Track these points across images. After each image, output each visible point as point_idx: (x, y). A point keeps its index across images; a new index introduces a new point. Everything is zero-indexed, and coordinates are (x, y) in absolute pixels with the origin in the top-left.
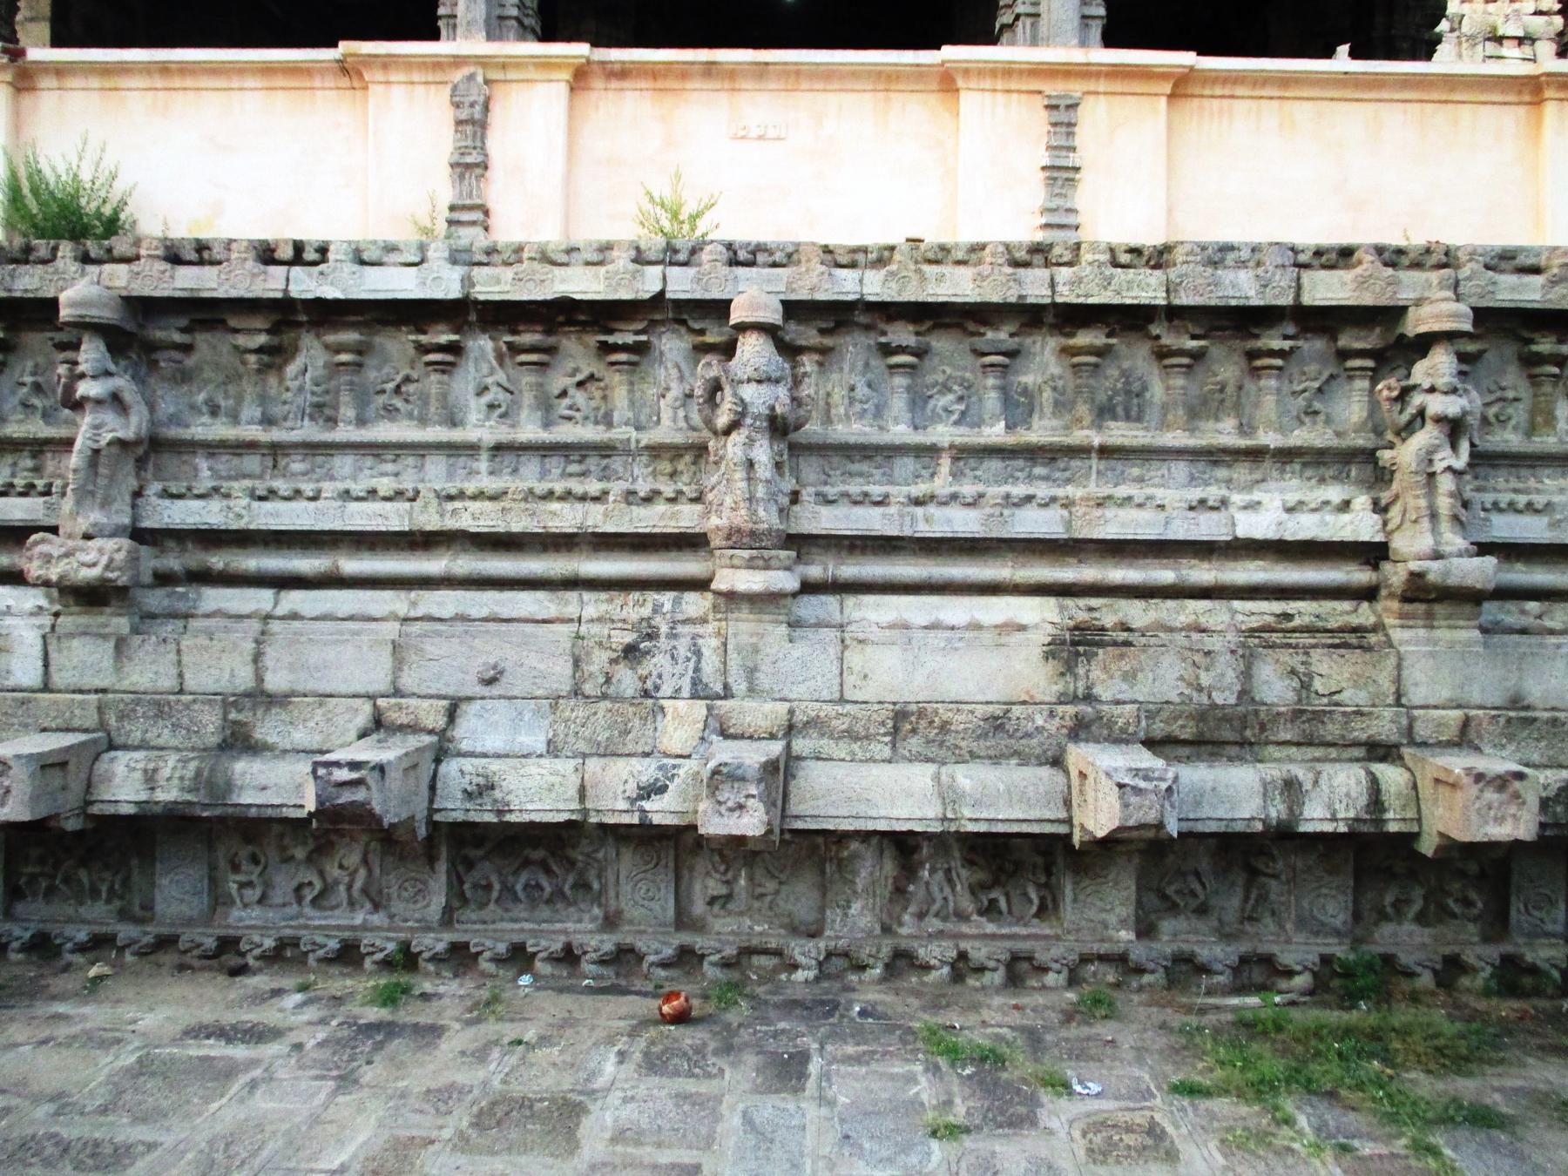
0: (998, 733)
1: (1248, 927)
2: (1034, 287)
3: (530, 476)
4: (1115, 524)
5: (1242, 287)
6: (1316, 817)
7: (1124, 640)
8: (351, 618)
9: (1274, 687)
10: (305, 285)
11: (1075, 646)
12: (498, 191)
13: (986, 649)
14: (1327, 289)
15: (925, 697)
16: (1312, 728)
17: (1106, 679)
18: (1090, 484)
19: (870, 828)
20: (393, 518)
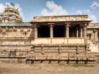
0: (67, 57)
1: (7, 33)
2: (67, 45)
3: (54, 50)
4: (70, 51)
5: (73, 45)
6: (75, 59)
7: (70, 54)
8: (6, 46)
9: (74, 56)
10: (48, 45)
11: (69, 55)
12: (51, 40)
13: (66, 55)
14: (75, 45)
15: (64, 56)
16: (75, 57)
17: (69, 55)
18: (69, 50)
19: (25, 25)
20: (50, 51)
